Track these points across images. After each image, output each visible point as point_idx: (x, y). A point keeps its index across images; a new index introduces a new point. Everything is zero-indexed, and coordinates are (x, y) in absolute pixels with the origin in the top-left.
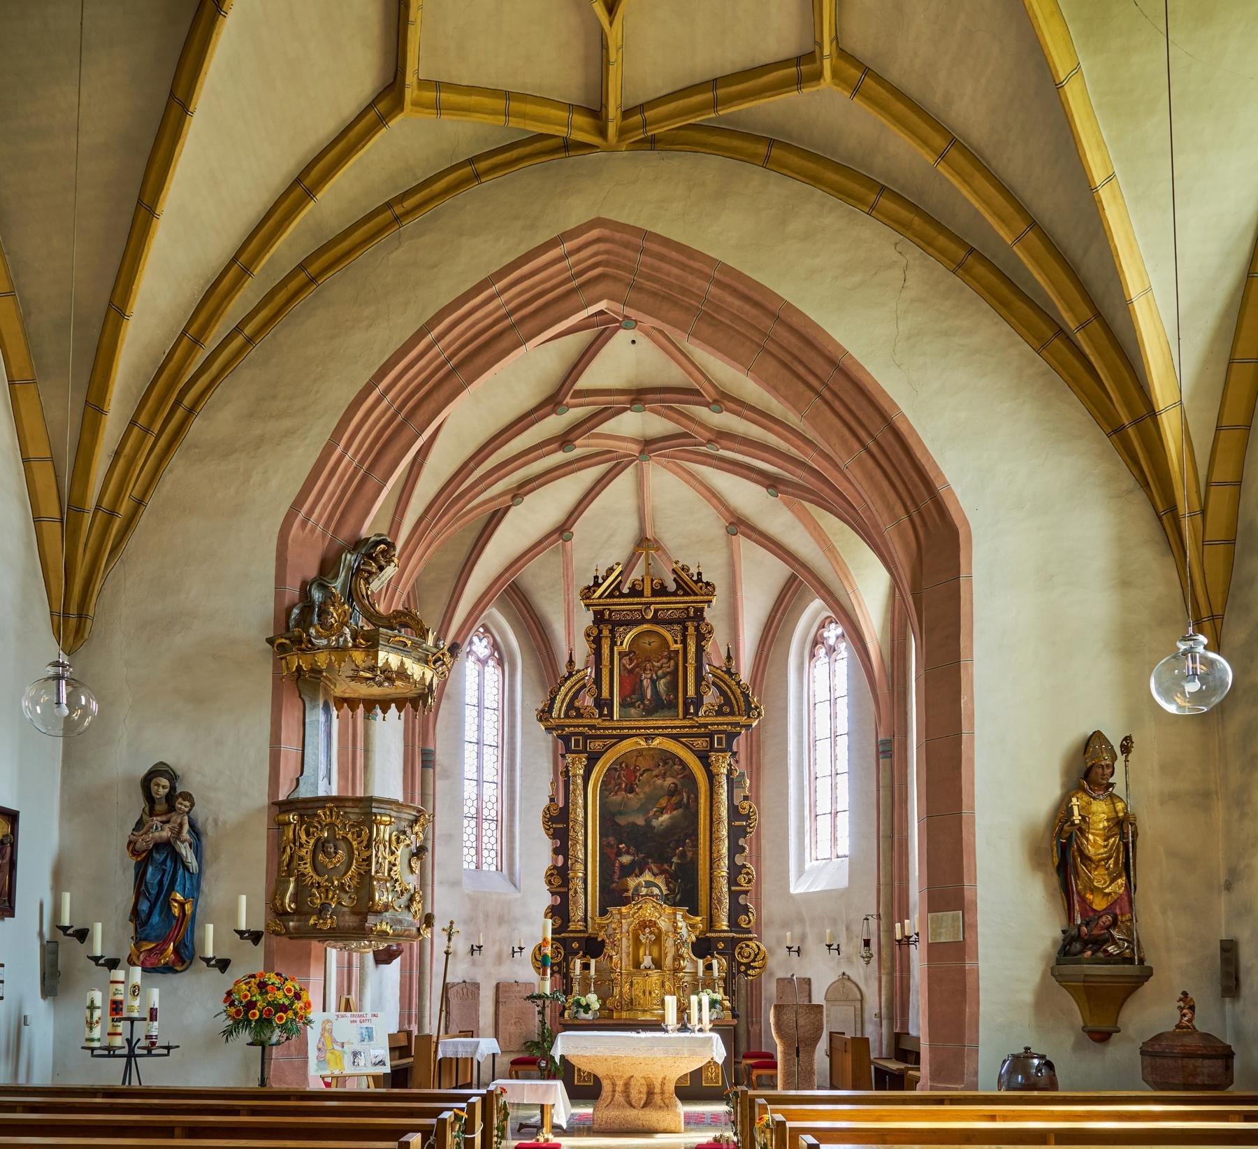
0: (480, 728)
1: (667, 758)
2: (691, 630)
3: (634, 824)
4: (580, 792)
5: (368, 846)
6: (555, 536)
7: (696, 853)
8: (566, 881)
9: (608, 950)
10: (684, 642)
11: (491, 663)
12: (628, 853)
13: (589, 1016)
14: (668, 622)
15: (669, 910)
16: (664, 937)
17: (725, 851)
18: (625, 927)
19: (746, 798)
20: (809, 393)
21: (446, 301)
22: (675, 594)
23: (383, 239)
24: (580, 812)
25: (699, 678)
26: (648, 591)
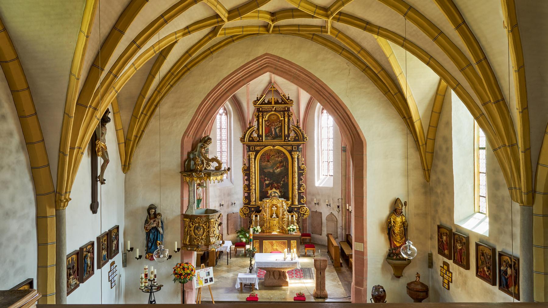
0: (221, 135)
1: (279, 152)
2: (286, 114)
4: (253, 163)
5: (208, 228)
7: (288, 181)
8: (250, 190)
10: (284, 117)
11: (224, 114)
14: (280, 111)
17: (297, 181)
19: (303, 164)
20: (324, 100)
21: (225, 76)
22: (281, 104)
23: (208, 58)
24: (254, 169)
25: (289, 128)
26: (273, 103)
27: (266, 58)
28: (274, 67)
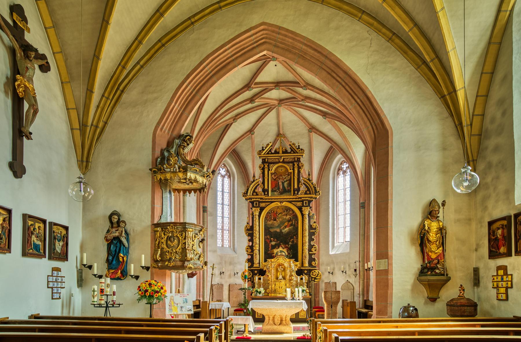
0: (223, 199)
1: (288, 209)
2: (296, 165)
3: (276, 231)
5: (185, 239)
6: (249, 133)
7: (297, 241)
8: (252, 251)
9: (267, 273)
10: (293, 169)
12: (274, 241)
13: (261, 295)
14: (289, 163)
15: (288, 260)
16: (286, 269)
18: (273, 266)
19: (315, 222)
22: (290, 153)
24: (257, 227)
25: (299, 181)
27: (263, 30)
28: (274, 42)
